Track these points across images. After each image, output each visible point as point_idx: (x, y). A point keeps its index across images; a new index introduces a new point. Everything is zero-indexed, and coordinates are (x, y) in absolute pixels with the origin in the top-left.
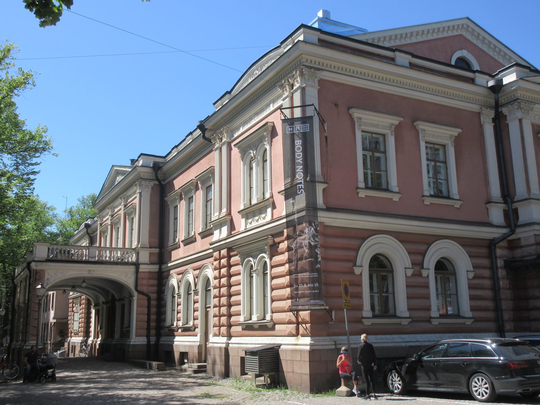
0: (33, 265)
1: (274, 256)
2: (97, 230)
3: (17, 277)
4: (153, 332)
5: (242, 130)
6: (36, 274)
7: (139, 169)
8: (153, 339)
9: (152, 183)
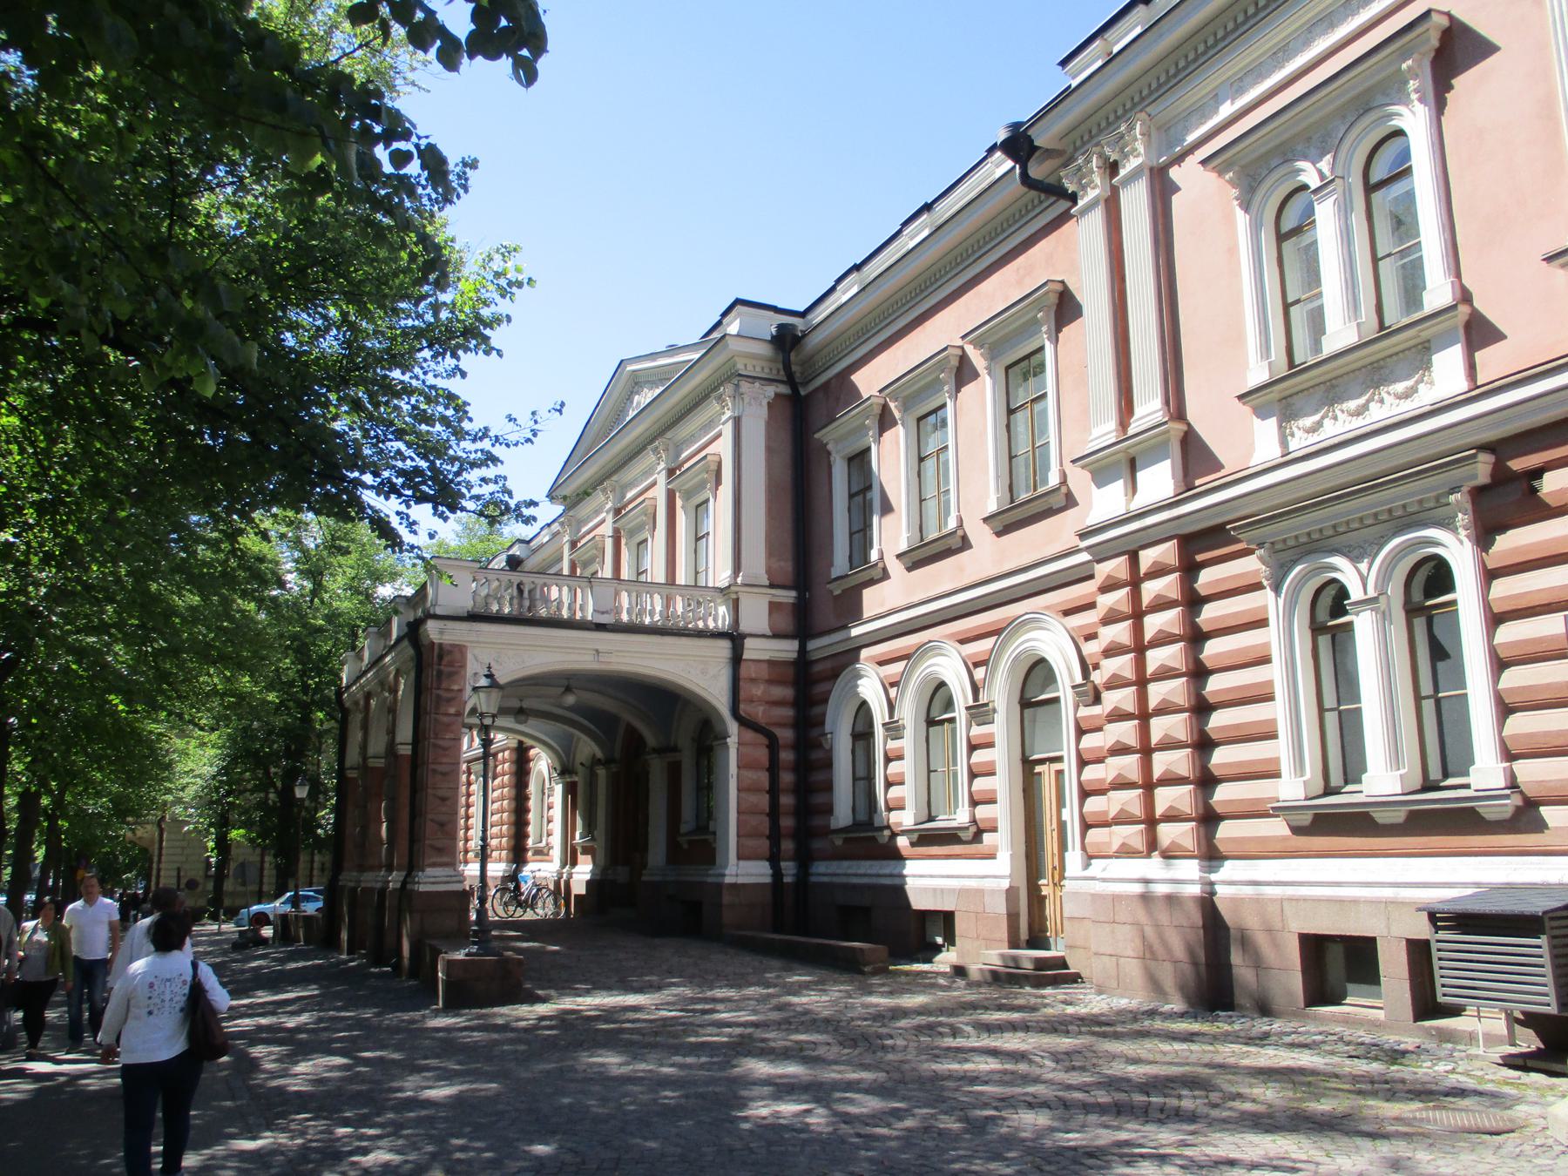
0: (432, 629)
1: (1503, 528)
2: (561, 559)
3: (348, 687)
4: (787, 845)
5: (1227, 110)
6: (441, 657)
7: (734, 346)
8: (789, 868)
9: (771, 391)
